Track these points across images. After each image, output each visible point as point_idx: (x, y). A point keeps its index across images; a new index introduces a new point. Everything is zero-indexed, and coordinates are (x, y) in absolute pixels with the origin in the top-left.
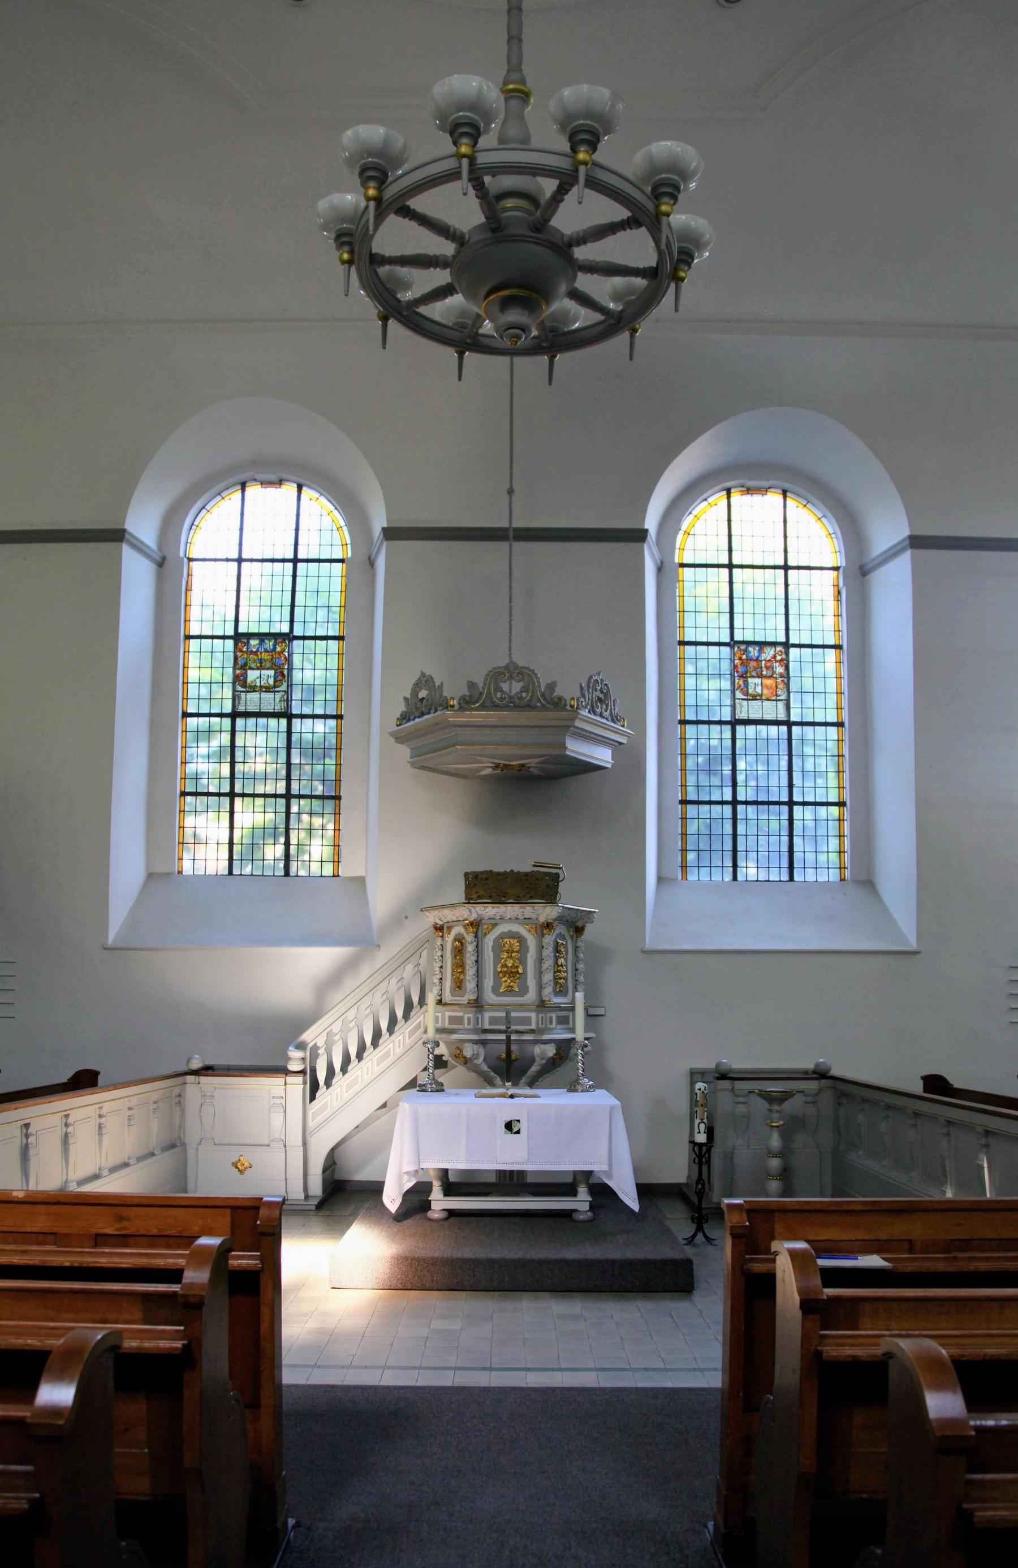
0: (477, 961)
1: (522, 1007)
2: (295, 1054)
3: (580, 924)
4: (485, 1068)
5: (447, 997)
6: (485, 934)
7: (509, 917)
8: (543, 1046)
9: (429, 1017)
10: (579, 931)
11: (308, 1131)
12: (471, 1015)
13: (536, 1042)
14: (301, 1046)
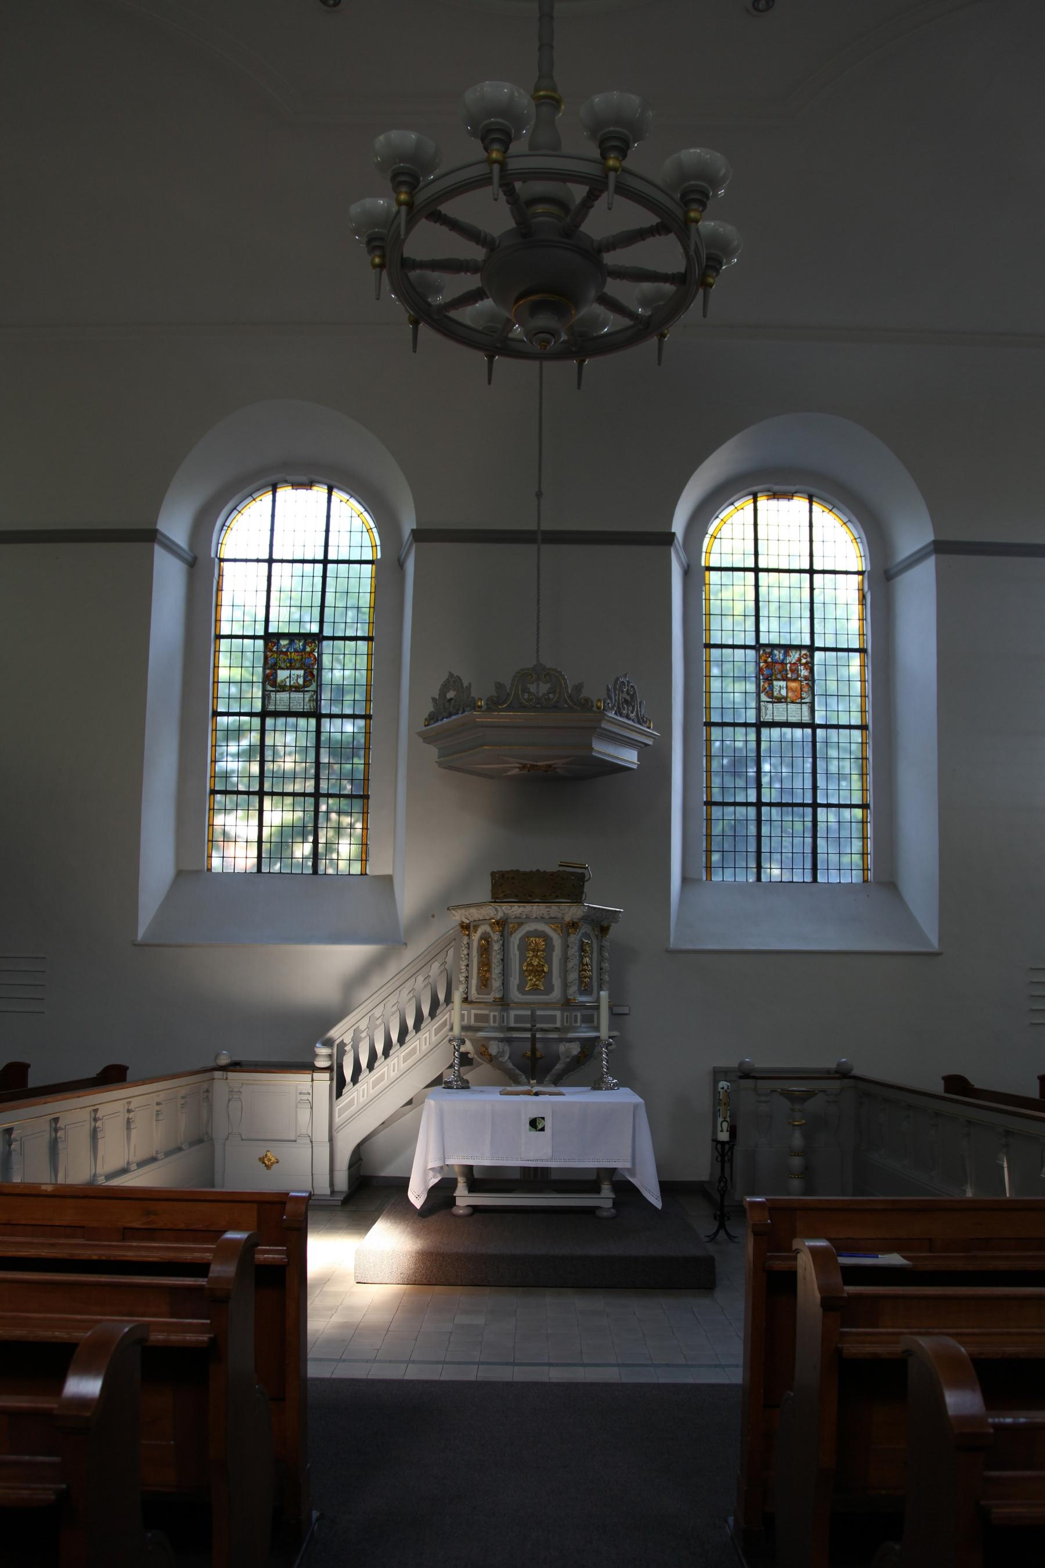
0: (502, 960)
1: (546, 1005)
2: (322, 1051)
3: (605, 924)
4: (510, 1065)
5: (473, 994)
6: (511, 933)
7: (534, 916)
8: (567, 1044)
10: (604, 930)
11: (335, 1127)
13: (561, 1040)
14: (329, 1043)
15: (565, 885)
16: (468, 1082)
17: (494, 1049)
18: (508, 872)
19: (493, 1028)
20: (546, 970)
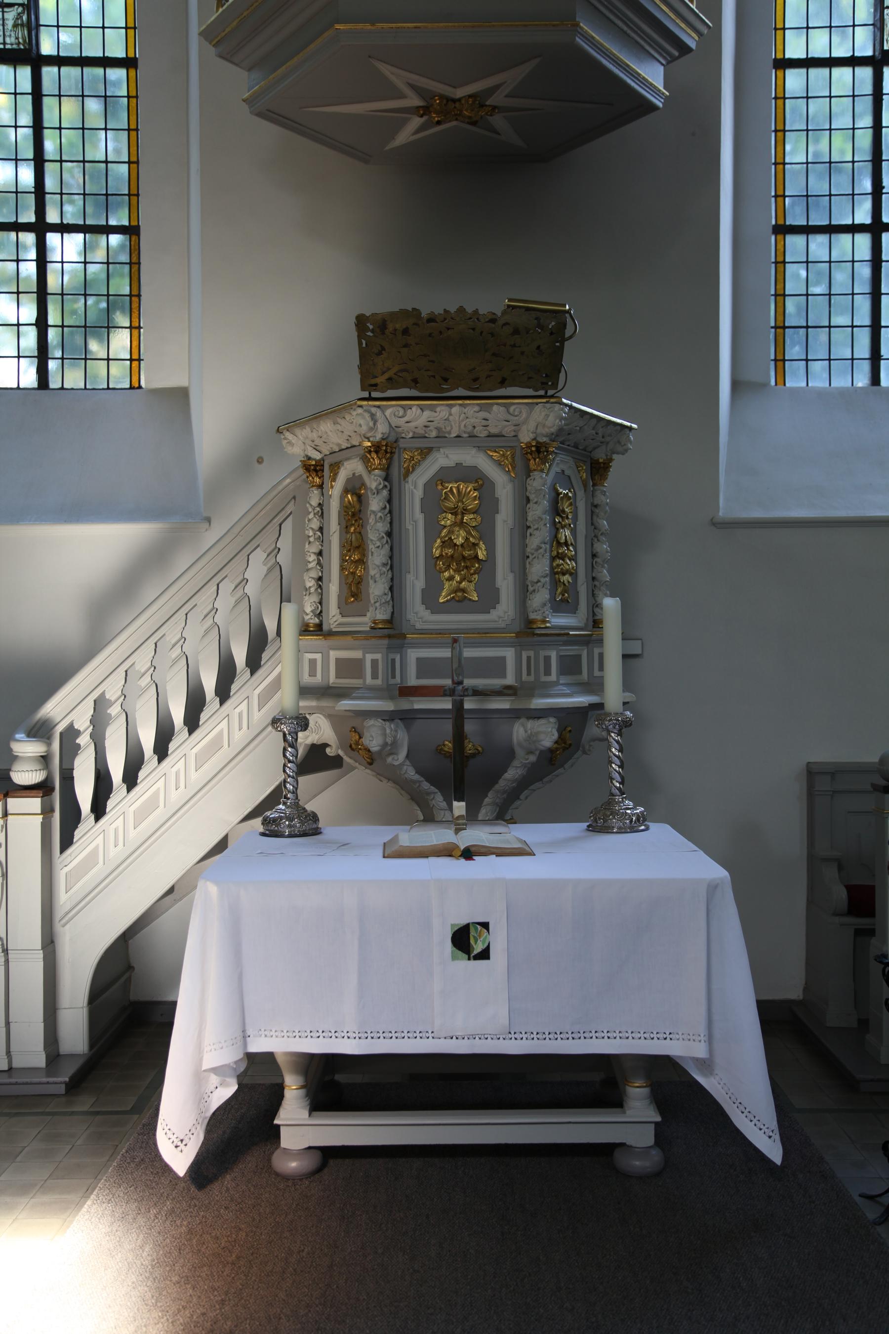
0: (389, 534)
1: (485, 636)
2: (27, 748)
3: (600, 455)
4: (411, 773)
5: (333, 617)
6: (407, 473)
7: (455, 427)
8: (530, 724)
9: (285, 664)
10: (598, 470)
11: (59, 913)
12: (378, 656)
13: (516, 714)
14: (41, 731)
15: (519, 353)
16: (314, 817)
17: (374, 737)
18: (392, 315)
19: (371, 689)
20: (481, 554)
